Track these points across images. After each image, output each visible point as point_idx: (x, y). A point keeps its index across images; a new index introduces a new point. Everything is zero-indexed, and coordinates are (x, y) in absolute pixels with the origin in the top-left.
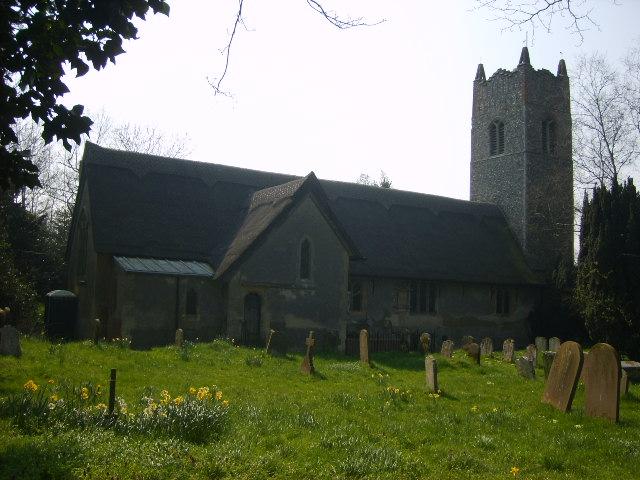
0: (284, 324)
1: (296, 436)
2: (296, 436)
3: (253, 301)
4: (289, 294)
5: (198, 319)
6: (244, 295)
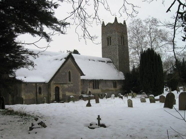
0: (65, 94)
1: (60, 123)
2: (60, 123)
3: (57, 89)
4: (66, 86)
5: (42, 95)
6: (54, 88)
